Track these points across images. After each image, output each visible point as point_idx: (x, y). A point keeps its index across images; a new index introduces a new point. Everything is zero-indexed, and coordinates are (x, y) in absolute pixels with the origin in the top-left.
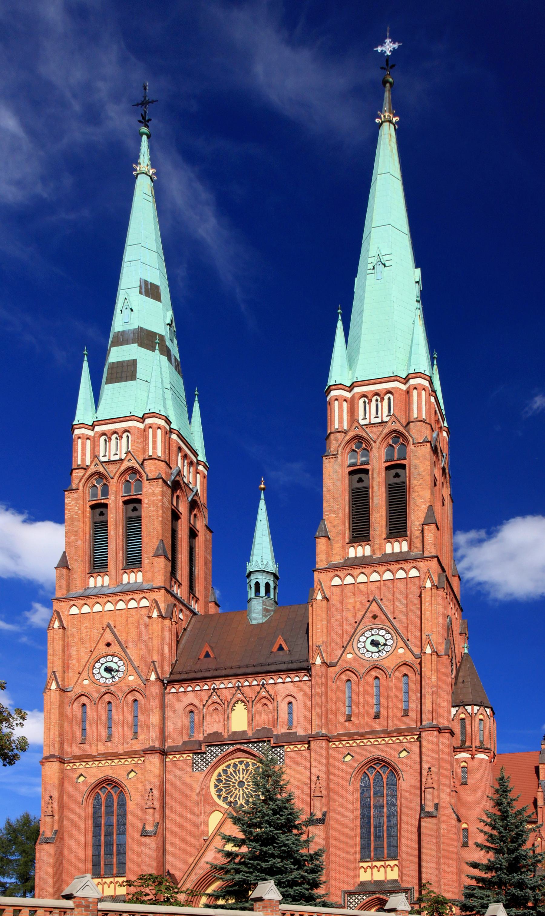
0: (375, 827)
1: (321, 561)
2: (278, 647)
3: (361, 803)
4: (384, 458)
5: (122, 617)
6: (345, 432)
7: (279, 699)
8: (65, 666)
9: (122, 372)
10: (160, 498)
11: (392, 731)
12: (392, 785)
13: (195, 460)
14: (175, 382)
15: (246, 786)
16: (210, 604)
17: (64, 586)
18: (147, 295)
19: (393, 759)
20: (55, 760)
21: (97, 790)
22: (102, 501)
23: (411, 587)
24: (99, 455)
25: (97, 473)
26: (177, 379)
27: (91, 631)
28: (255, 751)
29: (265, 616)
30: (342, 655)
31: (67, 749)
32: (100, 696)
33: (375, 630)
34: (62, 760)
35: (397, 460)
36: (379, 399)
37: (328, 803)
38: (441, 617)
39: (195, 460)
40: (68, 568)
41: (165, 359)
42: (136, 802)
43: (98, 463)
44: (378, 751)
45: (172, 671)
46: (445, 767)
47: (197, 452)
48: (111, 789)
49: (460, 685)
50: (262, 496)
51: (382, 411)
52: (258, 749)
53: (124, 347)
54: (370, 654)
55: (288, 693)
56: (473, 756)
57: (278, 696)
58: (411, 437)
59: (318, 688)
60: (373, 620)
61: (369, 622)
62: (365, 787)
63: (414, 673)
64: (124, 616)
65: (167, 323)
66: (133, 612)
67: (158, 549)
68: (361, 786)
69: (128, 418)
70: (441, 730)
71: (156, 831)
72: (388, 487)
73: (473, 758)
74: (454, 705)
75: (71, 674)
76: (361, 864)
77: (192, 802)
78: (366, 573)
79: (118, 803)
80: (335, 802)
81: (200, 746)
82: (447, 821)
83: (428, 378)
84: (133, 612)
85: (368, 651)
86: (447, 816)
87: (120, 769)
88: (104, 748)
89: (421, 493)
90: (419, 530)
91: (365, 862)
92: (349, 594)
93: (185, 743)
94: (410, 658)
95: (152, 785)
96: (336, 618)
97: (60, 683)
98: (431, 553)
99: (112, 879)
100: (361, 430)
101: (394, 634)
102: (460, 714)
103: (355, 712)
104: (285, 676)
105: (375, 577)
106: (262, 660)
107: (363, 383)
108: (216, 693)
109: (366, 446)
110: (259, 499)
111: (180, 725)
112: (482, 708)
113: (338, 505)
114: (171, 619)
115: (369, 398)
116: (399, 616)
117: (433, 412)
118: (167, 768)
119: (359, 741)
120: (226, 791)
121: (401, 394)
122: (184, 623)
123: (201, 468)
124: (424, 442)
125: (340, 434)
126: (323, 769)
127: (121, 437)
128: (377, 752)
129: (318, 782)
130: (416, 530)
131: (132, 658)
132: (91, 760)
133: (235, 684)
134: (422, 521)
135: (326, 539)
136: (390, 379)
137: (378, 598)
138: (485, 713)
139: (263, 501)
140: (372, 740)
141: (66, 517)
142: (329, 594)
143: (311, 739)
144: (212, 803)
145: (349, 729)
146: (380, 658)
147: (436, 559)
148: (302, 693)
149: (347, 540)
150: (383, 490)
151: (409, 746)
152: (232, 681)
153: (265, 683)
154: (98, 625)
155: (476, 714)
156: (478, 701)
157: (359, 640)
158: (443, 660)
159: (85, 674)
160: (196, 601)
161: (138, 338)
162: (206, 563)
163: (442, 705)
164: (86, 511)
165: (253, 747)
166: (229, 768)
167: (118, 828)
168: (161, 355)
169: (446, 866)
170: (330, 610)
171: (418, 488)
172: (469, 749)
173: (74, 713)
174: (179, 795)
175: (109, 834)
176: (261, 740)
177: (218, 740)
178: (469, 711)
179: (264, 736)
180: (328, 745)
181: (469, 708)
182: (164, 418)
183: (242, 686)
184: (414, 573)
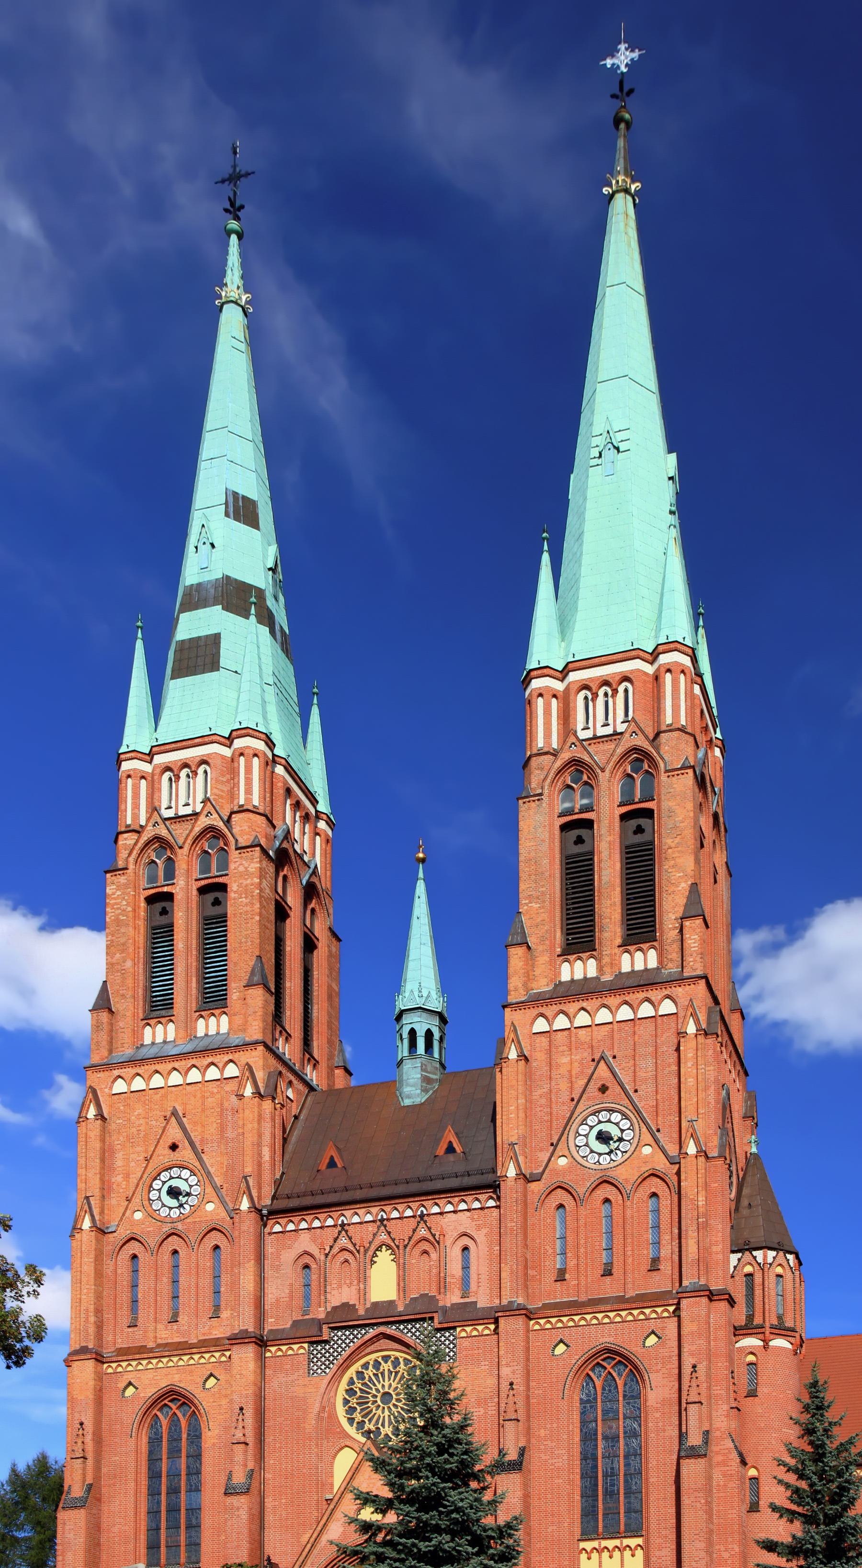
0: (605, 1475)
3: (581, 1430)
4: (618, 798)
5: (195, 1097)
6: (555, 754)
7: (448, 1242)
8: (106, 1187)
9: (197, 657)
11: (632, 1297)
12: (633, 1397)
15: (394, 1401)
18: (237, 518)
19: (634, 1350)
20: (89, 1356)
21: (155, 1411)
22: (165, 889)
23: (663, 1033)
25: (157, 839)
27: (147, 1123)
28: (408, 1338)
30: (549, 1160)
31: (108, 1337)
32: (160, 1240)
34: (99, 1358)
35: (640, 802)
38: (713, 1087)
40: (110, 1011)
42: (217, 1431)
43: (159, 820)
45: (275, 1193)
46: (720, 1364)
47: (317, 796)
49: (745, 1212)
51: (615, 714)
52: (414, 1334)
54: (597, 1156)
55: (462, 1230)
56: (766, 1342)
57: (447, 1236)
58: (662, 758)
60: (600, 1095)
62: (588, 1401)
63: (667, 1190)
67: (253, 973)
68: (581, 1399)
69: (206, 739)
73: (766, 1347)
75: (114, 1202)
76: (582, 1545)
77: (307, 1431)
78: (589, 1008)
79: (189, 1435)
80: (539, 1429)
81: (321, 1329)
82: (724, 1463)
83: (690, 652)
85: (592, 1151)
86: (724, 1455)
88: (167, 1334)
89: (678, 860)
92: (561, 1049)
93: (296, 1323)
95: (243, 1400)
96: (540, 1092)
97: (97, 1217)
98: (695, 970)
100: (580, 748)
101: (635, 1120)
104: (457, 1199)
105: (603, 1016)
106: (421, 1172)
108: (346, 1231)
111: (287, 1291)
112: (781, 1253)
113: (543, 886)
114: (274, 1098)
116: (643, 1087)
117: (698, 712)
118: (267, 1370)
120: (362, 1410)
123: (322, 825)
126: (520, 1369)
127: (195, 773)
128: (606, 1338)
129: (511, 1392)
130: (670, 929)
132: (145, 1356)
133: (377, 1215)
135: (524, 948)
137: (609, 1054)
138: (785, 1264)
140: (600, 1316)
141: (108, 920)
142: (529, 1048)
143: (500, 1314)
144: (339, 1433)
146: (613, 1164)
147: (704, 980)
148: (484, 1231)
150: (617, 857)
151: (661, 1325)
153: (425, 1212)
154: (158, 1112)
157: (577, 1132)
158: (716, 1166)
159: (136, 1200)
161: (222, 596)
163: (714, 1249)
164: (139, 907)
165: (406, 1331)
167: (188, 1480)
169: (723, 1548)
171: (673, 852)
173: (119, 1271)
174: (286, 1419)
175: (174, 1491)
177: (349, 1317)
178: (760, 1259)
180: (528, 1325)
181: (759, 1254)
182: (263, 736)
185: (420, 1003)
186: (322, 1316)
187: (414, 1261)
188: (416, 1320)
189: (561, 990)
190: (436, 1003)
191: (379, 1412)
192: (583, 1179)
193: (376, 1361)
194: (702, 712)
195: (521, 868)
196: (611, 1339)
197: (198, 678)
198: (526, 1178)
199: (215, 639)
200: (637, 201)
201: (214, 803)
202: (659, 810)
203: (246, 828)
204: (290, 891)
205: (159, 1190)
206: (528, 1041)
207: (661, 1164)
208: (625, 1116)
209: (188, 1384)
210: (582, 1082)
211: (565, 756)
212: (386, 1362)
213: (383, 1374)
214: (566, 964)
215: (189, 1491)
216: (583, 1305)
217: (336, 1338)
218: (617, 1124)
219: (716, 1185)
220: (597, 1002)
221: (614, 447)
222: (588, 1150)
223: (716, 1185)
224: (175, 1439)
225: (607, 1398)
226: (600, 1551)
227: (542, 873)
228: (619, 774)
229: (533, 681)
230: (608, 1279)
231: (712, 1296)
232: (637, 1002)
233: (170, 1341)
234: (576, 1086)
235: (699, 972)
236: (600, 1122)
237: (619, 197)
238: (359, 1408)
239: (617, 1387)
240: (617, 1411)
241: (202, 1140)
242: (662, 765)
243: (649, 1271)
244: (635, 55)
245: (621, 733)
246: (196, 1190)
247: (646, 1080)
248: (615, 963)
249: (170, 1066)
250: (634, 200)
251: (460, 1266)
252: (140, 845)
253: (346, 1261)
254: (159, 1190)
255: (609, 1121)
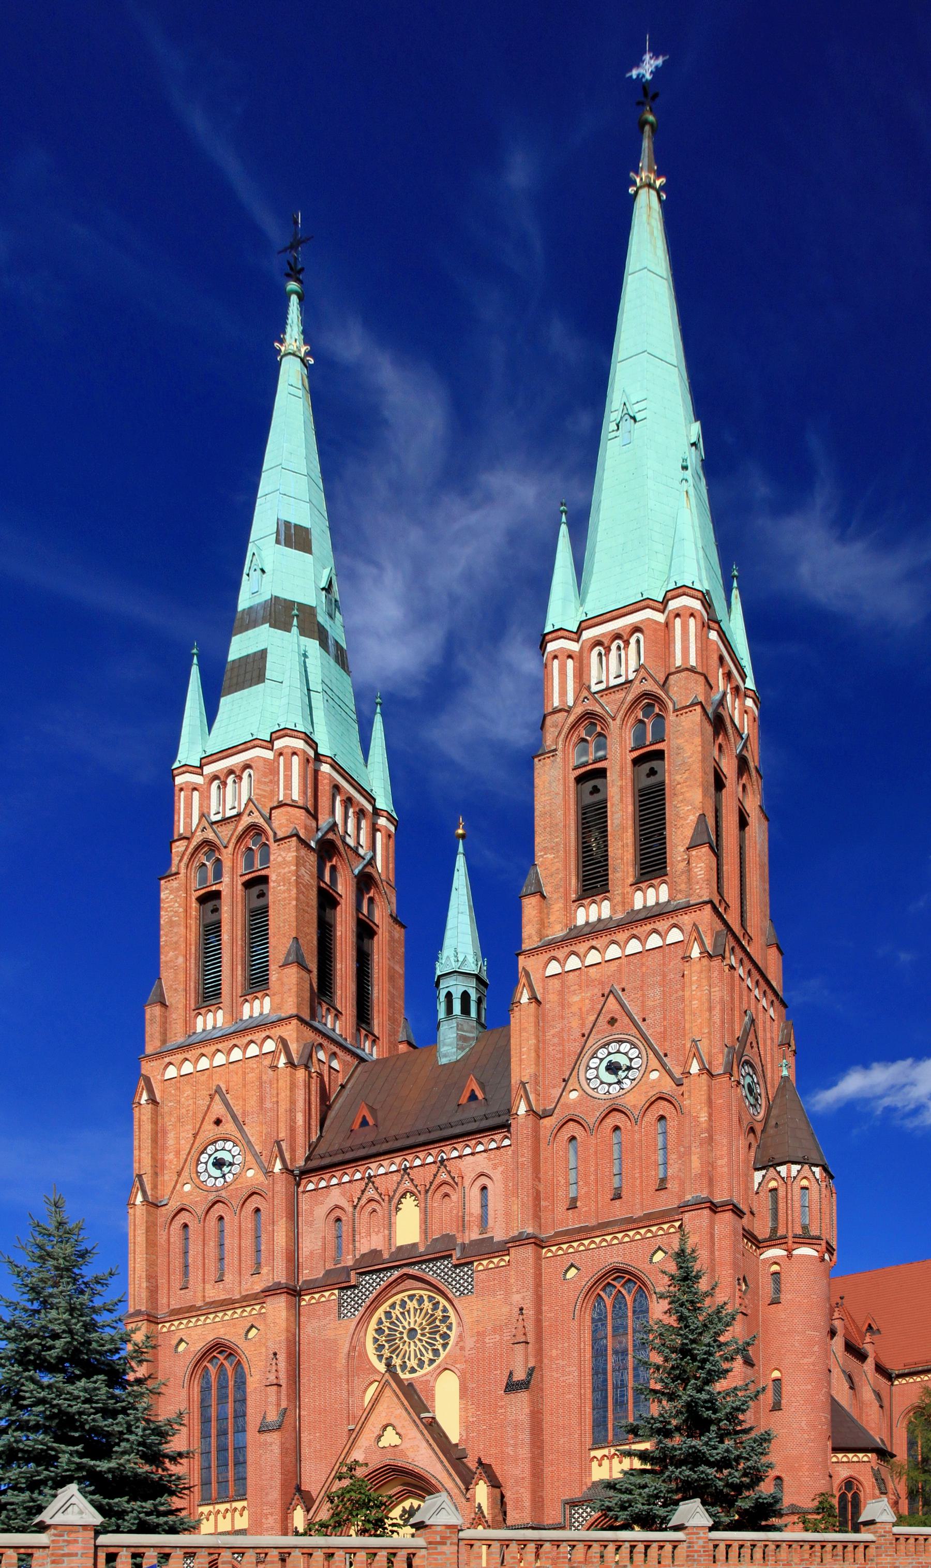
0: (615, 1387)
1: (530, 935)
2: (468, 1095)
3: (593, 1348)
4: (631, 743)
5: (237, 1074)
6: (568, 711)
7: (467, 1183)
8: (159, 1165)
9: (246, 673)
10: (294, 868)
11: (639, 1217)
12: (642, 1312)
13: (370, 808)
14: (334, 680)
15: (419, 1336)
16: (401, 1046)
17: (157, 1034)
18: (288, 544)
19: (641, 1267)
20: (141, 1318)
21: (205, 1363)
22: (214, 888)
23: (670, 961)
24: (209, 813)
25: (206, 842)
26: (339, 677)
27: (195, 1103)
28: (430, 1276)
29: (462, 1049)
30: (561, 1095)
31: (163, 1300)
32: (207, 1208)
33: (613, 1045)
34: (151, 1319)
35: (651, 745)
36: (622, 645)
37: (539, 1353)
38: (718, 1008)
39: (369, 808)
40: (163, 1004)
41: (312, 645)
42: (258, 1377)
43: (207, 825)
44: (618, 1255)
45: (311, 1154)
46: (724, 1272)
47: (374, 794)
48: (226, 1358)
49: (771, 1131)
50: (461, 849)
51: (627, 664)
52: (435, 1272)
53: (251, 633)
54: (606, 1087)
55: (479, 1170)
56: (790, 1251)
57: (465, 1178)
58: (670, 699)
59: (523, 1156)
60: (610, 1027)
61: (604, 1031)
62: (600, 1320)
63: (674, 1111)
64: (240, 1072)
65: (322, 587)
66: (253, 1064)
67: (289, 954)
68: (593, 1318)
69: (249, 745)
70: (717, 1207)
71: (282, 1422)
72: (637, 794)
73: (790, 1256)
74: (758, 1166)
75: (166, 1178)
76: (593, 1453)
77: (338, 1370)
78: (598, 946)
79: (235, 1382)
80: (551, 1350)
81: (349, 1275)
84: (253, 1064)
85: (602, 1083)
87: (235, 1325)
88: (214, 1293)
89: (688, 795)
90: (684, 859)
91: (599, 1448)
92: (572, 988)
93: (328, 1273)
94: (668, 1086)
95: (277, 1346)
96: (552, 1032)
97: (149, 1193)
98: (701, 897)
99: (227, 1506)
100: (592, 701)
101: (642, 1048)
102: (768, 1182)
103: (583, 1191)
104: (474, 1142)
105: (614, 952)
106: (443, 1120)
107: (596, 620)
108: (373, 1183)
109: (602, 729)
110: (455, 853)
111: (320, 1244)
112: (806, 1167)
113: (557, 837)
114: (307, 1067)
115: (606, 645)
116: (651, 1015)
117: (715, 657)
118: (302, 1318)
119: (589, 1241)
120: (390, 1346)
121: (655, 630)
122: (340, 1075)
123: (382, 821)
124: (692, 705)
125: (560, 714)
126: (529, 1294)
127: (240, 778)
128: (615, 1258)
129: (521, 1317)
130: (679, 862)
131: (252, 1140)
132: (194, 1314)
133: (400, 1164)
134: (687, 842)
135: (538, 897)
136: (638, 606)
137: (617, 988)
138: (810, 1176)
139: (462, 855)
140: (608, 1238)
141: (162, 922)
142: (542, 991)
143: (510, 1245)
144: (368, 1369)
145: (574, 1223)
146: (622, 1092)
147: (709, 905)
148: (500, 1169)
149: (574, 896)
150: (629, 800)
152: (395, 1160)
153: (445, 1157)
154: (205, 1092)
155: (795, 1178)
156: (799, 1155)
157: (588, 1066)
158: (721, 1083)
159: (185, 1174)
160: (374, 1041)
161: (270, 614)
162: (392, 978)
163: (719, 1162)
164: (191, 908)
165: (427, 1270)
166: (394, 1309)
167: (235, 1422)
168: (302, 638)
170: (543, 1020)
171: (681, 788)
172: (783, 1241)
173: (172, 1240)
174: (319, 1360)
175: (222, 1433)
176: (437, 1255)
177: (375, 1262)
178: (784, 1174)
179: (443, 1247)
180: (541, 1254)
181: (783, 1169)
182: (302, 736)
183: (411, 1168)
184: (675, 936)
185: (454, 966)
186: (350, 1263)
187: (435, 1205)
188: (437, 1259)
189: (573, 934)
190: (471, 967)
191: (406, 1347)
192: (593, 1110)
193: (402, 1300)
194: (721, 658)
195: (536, 822)
196: (620, 1259)
197: (246, 691)
198: (536, 1115)
199: (263, 654)
200: (664, 197)
201: (256, 802)
202: (669, 749)
203: (284, 821)
204: (340, 880)
205: (206, 1163)
206: (541, 985)
207: (668, 1086)
208: (634, 1046)
209: (233, 1336)
210: (593, 1018)
211: (579, 710)
212: (411, 1301)
213: (409, 1312)
214: (582, 909)
215: (236, 1431)
216: (593, 1228)
217: (364, 1283)
218: (626, 1054)
219: (721, 1101)
220: (606, 940)
221: (631, 417)
222: (599, 1082)
223: (721, 1101)
224: (223, 1387)
225: (617, 1315)
226: (610, 1458)
227: (557, 824)
228: (631, 721)
229: (549, 645)
230: (618, 1202)
231: (714, 1208)
232: (645, 934)
233: (217, 1299)
234: (587, 1022)
235: (706, 899)
236: (610, 1054)
237: (643, 193)
238: (387, 1346)
239: (626, 1305)
240: (626, 1328)
241: (244, 1113)
242: (670, 706)
243: (657, 1190)
244: (660, 61)
245: (631, 681)
246: (238, 1160)
247: (655, 1008)
248: (627, 901)
249: (213, 1048)
250: (659, 197)
251: (479, 1205)
252: (190, 850)
253: (374, 1211)
254: (206, 1163)
255: (618, 1052)
